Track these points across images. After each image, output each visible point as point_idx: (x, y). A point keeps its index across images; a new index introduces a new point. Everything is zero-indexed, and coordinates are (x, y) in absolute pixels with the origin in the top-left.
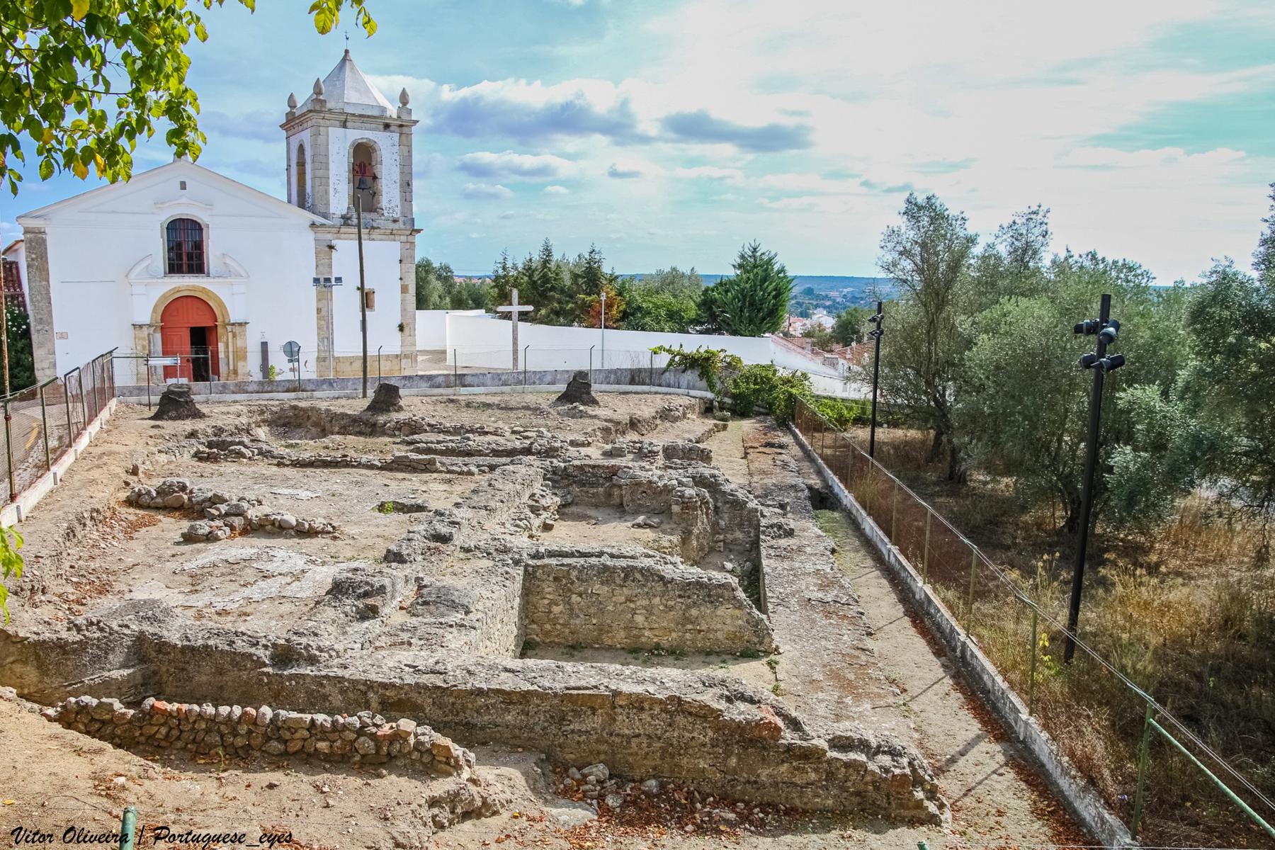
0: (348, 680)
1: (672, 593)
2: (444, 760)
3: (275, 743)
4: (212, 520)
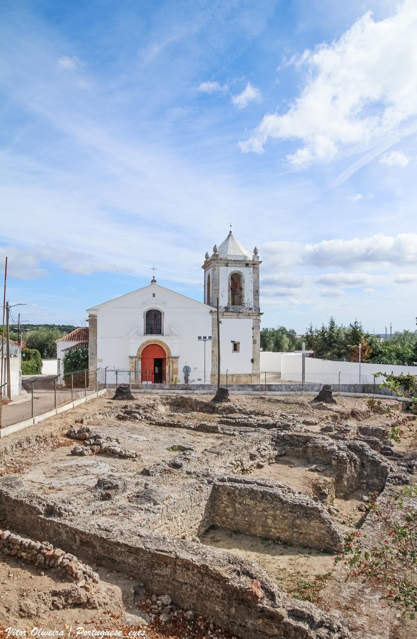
0: (69, 527)
1: (286, 509)
2: (71, 574)
3: (6, 549)
4: (86, 446)
